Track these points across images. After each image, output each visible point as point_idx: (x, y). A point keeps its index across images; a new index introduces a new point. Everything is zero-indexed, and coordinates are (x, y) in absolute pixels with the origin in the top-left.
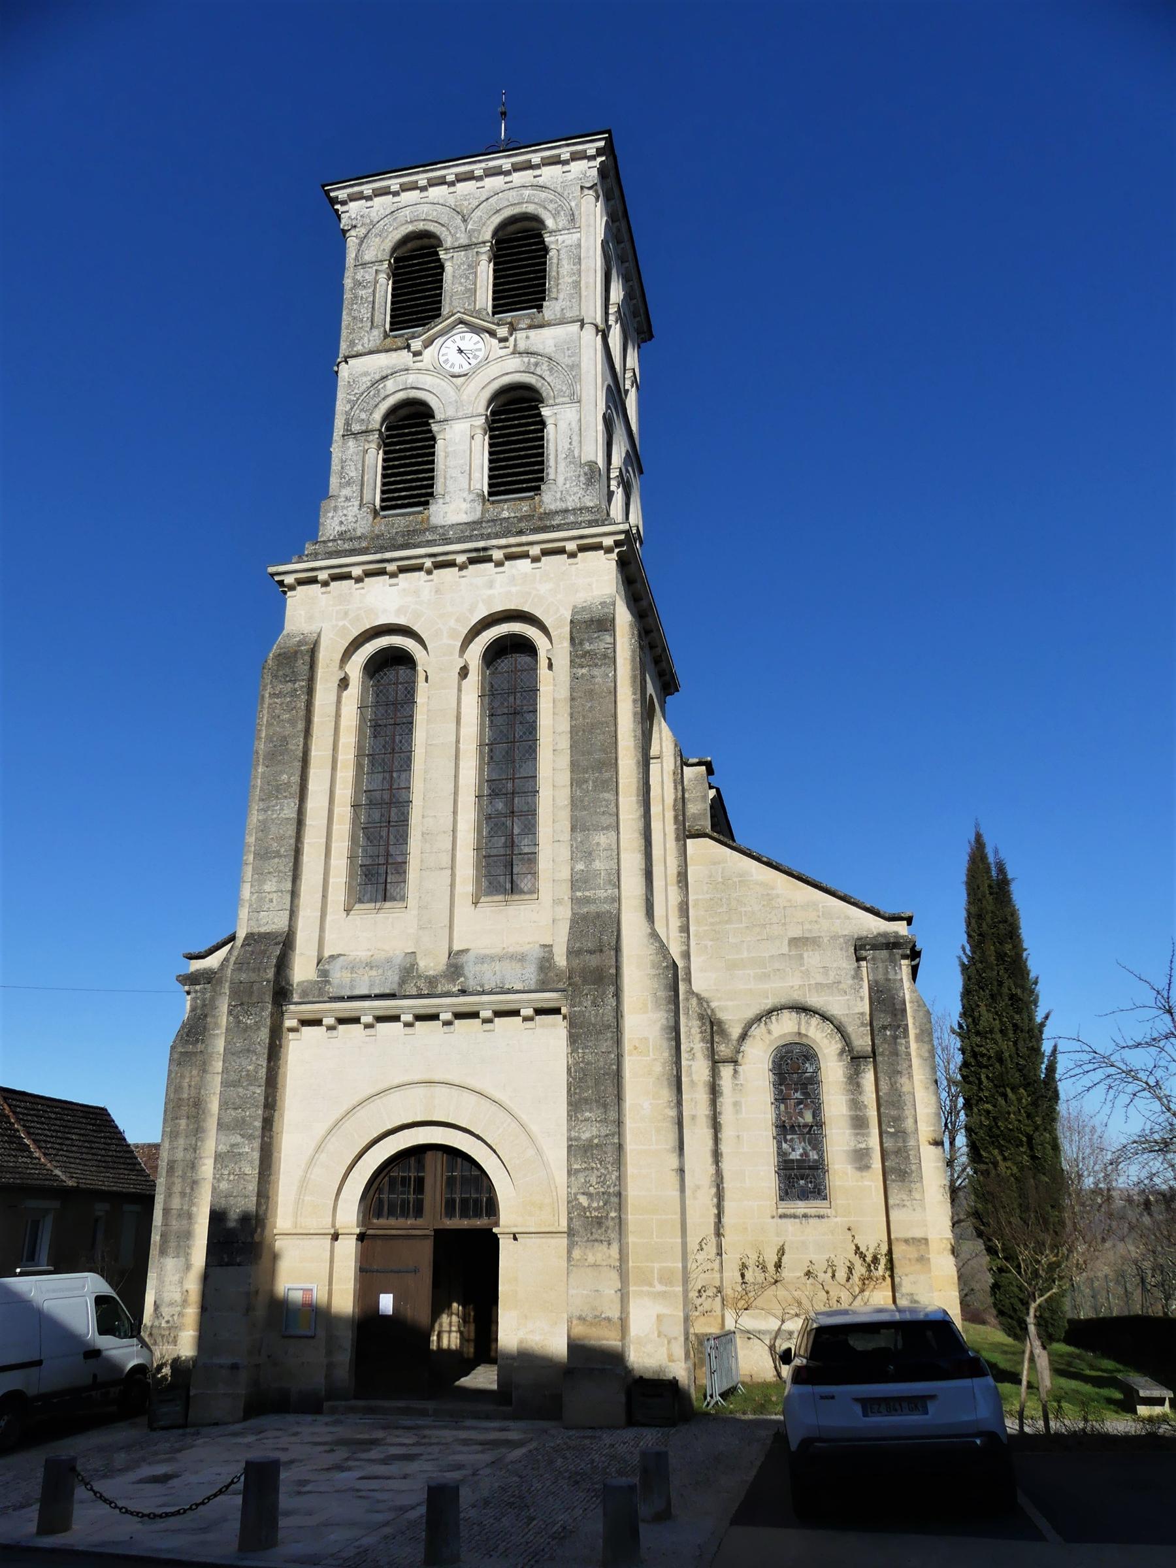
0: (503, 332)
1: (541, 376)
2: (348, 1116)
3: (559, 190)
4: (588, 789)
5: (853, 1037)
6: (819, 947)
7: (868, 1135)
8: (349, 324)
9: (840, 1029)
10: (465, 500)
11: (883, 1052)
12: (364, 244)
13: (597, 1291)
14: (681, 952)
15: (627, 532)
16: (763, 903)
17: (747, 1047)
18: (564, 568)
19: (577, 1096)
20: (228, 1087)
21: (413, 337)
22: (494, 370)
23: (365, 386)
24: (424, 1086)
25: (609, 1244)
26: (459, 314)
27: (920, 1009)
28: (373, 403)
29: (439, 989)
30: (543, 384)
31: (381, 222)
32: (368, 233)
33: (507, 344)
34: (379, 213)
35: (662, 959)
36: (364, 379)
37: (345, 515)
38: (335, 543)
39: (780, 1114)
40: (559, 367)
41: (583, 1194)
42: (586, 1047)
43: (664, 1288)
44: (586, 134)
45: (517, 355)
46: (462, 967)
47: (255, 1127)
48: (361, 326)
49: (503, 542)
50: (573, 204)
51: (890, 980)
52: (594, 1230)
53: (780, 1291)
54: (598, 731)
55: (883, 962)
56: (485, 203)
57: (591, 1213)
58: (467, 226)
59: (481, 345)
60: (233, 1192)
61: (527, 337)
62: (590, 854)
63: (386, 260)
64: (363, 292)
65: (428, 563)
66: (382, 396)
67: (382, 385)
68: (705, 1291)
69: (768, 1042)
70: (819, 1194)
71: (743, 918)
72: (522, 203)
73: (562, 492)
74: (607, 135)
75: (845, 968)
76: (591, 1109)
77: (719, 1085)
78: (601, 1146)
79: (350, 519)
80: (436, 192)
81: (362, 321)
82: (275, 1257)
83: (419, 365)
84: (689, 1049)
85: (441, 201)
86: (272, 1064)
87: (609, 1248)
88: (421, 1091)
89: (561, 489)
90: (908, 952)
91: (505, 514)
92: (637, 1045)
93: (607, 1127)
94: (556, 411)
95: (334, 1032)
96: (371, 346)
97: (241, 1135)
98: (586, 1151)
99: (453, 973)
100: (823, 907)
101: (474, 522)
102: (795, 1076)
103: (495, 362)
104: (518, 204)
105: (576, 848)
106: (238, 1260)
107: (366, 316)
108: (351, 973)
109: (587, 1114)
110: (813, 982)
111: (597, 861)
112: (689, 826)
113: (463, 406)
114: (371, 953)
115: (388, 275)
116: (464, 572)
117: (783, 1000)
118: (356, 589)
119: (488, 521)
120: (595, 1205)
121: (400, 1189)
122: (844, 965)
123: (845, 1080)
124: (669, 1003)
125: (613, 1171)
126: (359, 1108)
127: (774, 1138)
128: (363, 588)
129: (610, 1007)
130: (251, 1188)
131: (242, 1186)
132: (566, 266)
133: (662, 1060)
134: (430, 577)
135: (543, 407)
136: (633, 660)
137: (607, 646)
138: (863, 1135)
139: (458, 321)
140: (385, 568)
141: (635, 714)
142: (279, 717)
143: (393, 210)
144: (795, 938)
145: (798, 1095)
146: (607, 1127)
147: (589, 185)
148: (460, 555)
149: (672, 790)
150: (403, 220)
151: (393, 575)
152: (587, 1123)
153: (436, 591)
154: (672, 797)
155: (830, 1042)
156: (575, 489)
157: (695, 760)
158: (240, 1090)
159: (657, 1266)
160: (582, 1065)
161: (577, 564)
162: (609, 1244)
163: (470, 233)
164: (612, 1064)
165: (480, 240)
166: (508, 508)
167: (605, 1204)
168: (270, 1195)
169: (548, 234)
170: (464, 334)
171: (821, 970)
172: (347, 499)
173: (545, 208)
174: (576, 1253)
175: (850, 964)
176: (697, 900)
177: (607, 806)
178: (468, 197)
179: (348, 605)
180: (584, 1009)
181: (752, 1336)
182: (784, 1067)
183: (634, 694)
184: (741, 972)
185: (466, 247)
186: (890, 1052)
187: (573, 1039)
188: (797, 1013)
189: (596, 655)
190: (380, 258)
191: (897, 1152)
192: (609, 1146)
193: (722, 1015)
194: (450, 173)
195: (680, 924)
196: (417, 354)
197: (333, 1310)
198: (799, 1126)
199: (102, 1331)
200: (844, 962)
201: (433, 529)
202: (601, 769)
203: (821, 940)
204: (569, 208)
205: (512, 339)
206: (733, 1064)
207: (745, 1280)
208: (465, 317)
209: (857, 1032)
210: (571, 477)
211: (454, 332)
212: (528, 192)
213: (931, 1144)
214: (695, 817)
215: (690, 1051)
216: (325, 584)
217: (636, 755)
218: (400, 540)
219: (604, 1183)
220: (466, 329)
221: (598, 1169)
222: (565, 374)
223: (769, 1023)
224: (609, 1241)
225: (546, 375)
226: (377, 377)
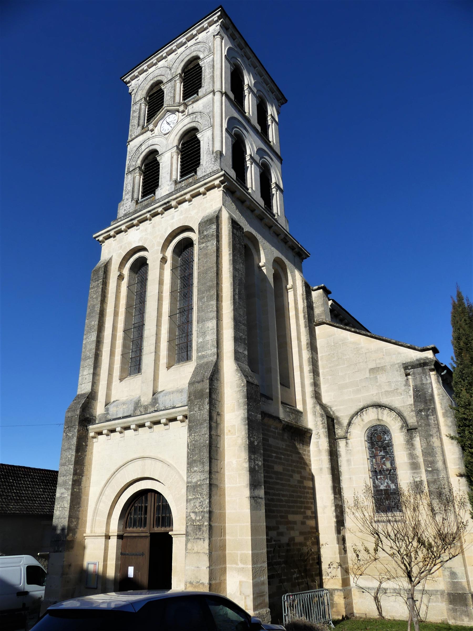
1: (197, 122)
2: (113, 477)
3: (205, 41)
5: (408, 418)
6: (385, 371)
7: (420, 473)
9: (400, 414)
10: (168, 185)
11: (421, 424)
13: (198, 567)
14: (311, 383)
15: (223, 175)
16: (354, 352)
17: (352, 429)
18: (201, 201)
19: (191, 459)
20: (61, 466)
24: (141, 460)
25: (204, 540)
27: (444, 398)
29: (149, 411)
30: (198, 125)
33: (184, 113)
35: (241, 382)
39: (373, 465)
40: (204, 115)
41: (193, 512)
42: (196, 433)
43: (243, 566)
44: (211, 13)
46: (158, 399)
47: (69, 484)
49: (174, 196)
51: (424, 384)
52: (197, 533)
53: (378, 564)
54: (209, 272)
55: (419, 375)
57: (196, 523)
60: (60, 516)
62: (205, 333)
66: (140, 153)
68: (332, 565)
69: (362, 426)
70: (398, 508)
71: (345, 362)
75: (400, 381)
76: (197, 465)
77: (339, 451)
78: (201, 485)
79: (128, 207)
80: (161, 64)
82: (84, 548)
83: (153, 135)
84: (317, 433)
85: (163, 66)
86: (80, 454)
87: (204, 543)
88: (140, 462)
90: (433, 367)
92: (230, 430)
93: (204, 475)
95: (109, 437)
97: (65, 488)
98: (194, 489)
99: (154, 402)
100: (386, 350)
102: (380, 443)
105: (199, 331)
106: (60, 549)
109: (195, 469)
110: (383, 391)
111: (208, 336)
112: (316, 320)
115: (145, 104)
116: (163, 215)
117: (369, 402)
120: (198, 518)
121: (139, 513)
122: (399, 379)
123: (405, 443)
124: (245, 405)
125: (206, 499)
126: (117, 473)
127: (370, 478)
129: (206, 410)
130: (66, 514)
131: (63, 513)
133: (242, 437)
137: (213, 230)
138: (418, 473)
139: (166, 111)
141: (230, 260)
144: (372, 369)
145: (382, 453)
146: (204, 475)
147: (216, 34)
149: (302, 303)
151: (137, 225)
152: (195, 473)
154: (302, 306)
155: (395, 422)
156: (210, 165)
157: (316, 287)
158: (66, 467)
159: (239, 552)
160: (193, 442)
162: (204, 540)
164: (206, 441)
167: (202, 518)
168: (80, 517)
171: (387, 384)
172: (127, 199)
174: (189, 545)
175: (403, 378)
176: (322, 356)
177: (212, 308)
180: (195, 412)
181: (364, 591)
182: (373, 439)
183: (230, 251)
184: (346, 390)
185: (170, 80)
186: (425, 424)
187: (190, 429)
188: (376, 408)
189: (208, 236)
191: (434, 482)
192: (205, 486)
193: (338, 414)
194: (164, 53)
195: (309, 369)
196: (152, 130)
197: (107, 575)
198: (384, 470)
199: (29, 582)
200: (399, 377)
202: (210, 290)
203: (386, 367)
206: (345, 439)
207: (359, 559)
208: (168, 108)
209: (409, 415)
210: (209, 160)
211: (166, 116)
213: (458, 476)
214: (319, 315)
215: (318, 434)
217: (230, 281)
219: (202, 506)
220: (170, 114)
221: (199, 499)
223: (362, 415)
224: (204, 538)
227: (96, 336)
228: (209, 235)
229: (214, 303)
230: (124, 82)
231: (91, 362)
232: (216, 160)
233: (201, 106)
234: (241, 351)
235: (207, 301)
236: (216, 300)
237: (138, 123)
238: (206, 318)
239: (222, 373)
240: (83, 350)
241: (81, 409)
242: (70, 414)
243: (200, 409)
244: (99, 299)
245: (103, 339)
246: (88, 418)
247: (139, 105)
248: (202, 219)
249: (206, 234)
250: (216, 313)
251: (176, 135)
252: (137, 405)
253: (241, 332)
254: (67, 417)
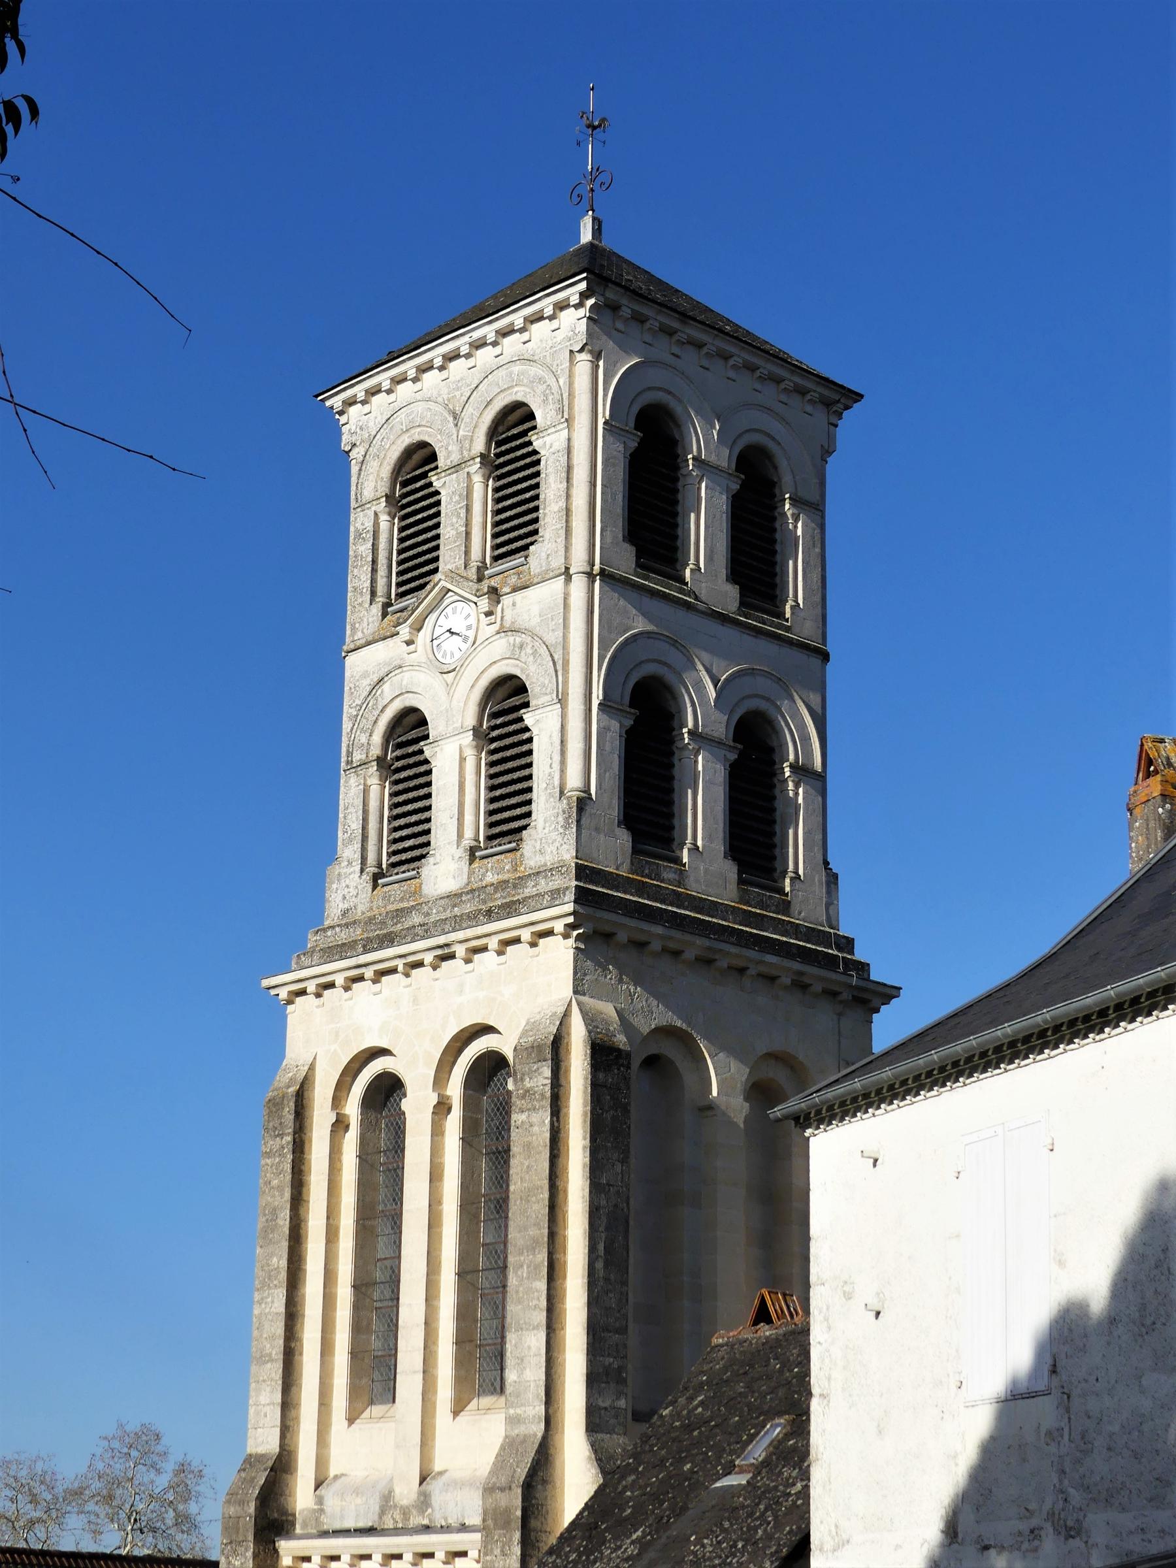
4: (523, 1277)
22: (481, 660)
46: (430, 1495)
54: (534, 1199)
58: (458, 431)
62: (522, 1360)
63: (382, 497)
65: (400, 964)
66: (380, 708)
67: (379, 691)
94: (537, 717)
103: (483, 646)
104: (508, 388)
108: (341, 1500)
111: (528, 1370)
114: (367, 1474)
115: (389, 514)
132: (553, 486)
136: (585, 1092)
142: (270, 1182)
147: (578, 348)
148: (427, 952)
178: (460, 384)
180: (494, 1558)
202: (534, 1249)
211: (446, 602)
227: (284, 1301)
228: (535, 1092)
229: (542, 1285)
231: (275, 1370)
232: (566, 827)
233: (535, 610)
234: (607, 1404)
235: (528, 1278)
236: (546, 1280)
237: (372, 586)
238: (525, 1323)
239: (558, 1463)
240: (255, 1333)
241: (258, 1502)
242: (232, 1511)
243: (504, 1554)
244: (287, 1195)
245: (303, 1305)
246: (276, 1520)
247: (371, 514)
248: (524, 1033)
249: (528, 1085)
250: (545, 1313)
251: (472, 686)
252: (387, 1502)
253: (609, 1355)
254: (227, 1516)
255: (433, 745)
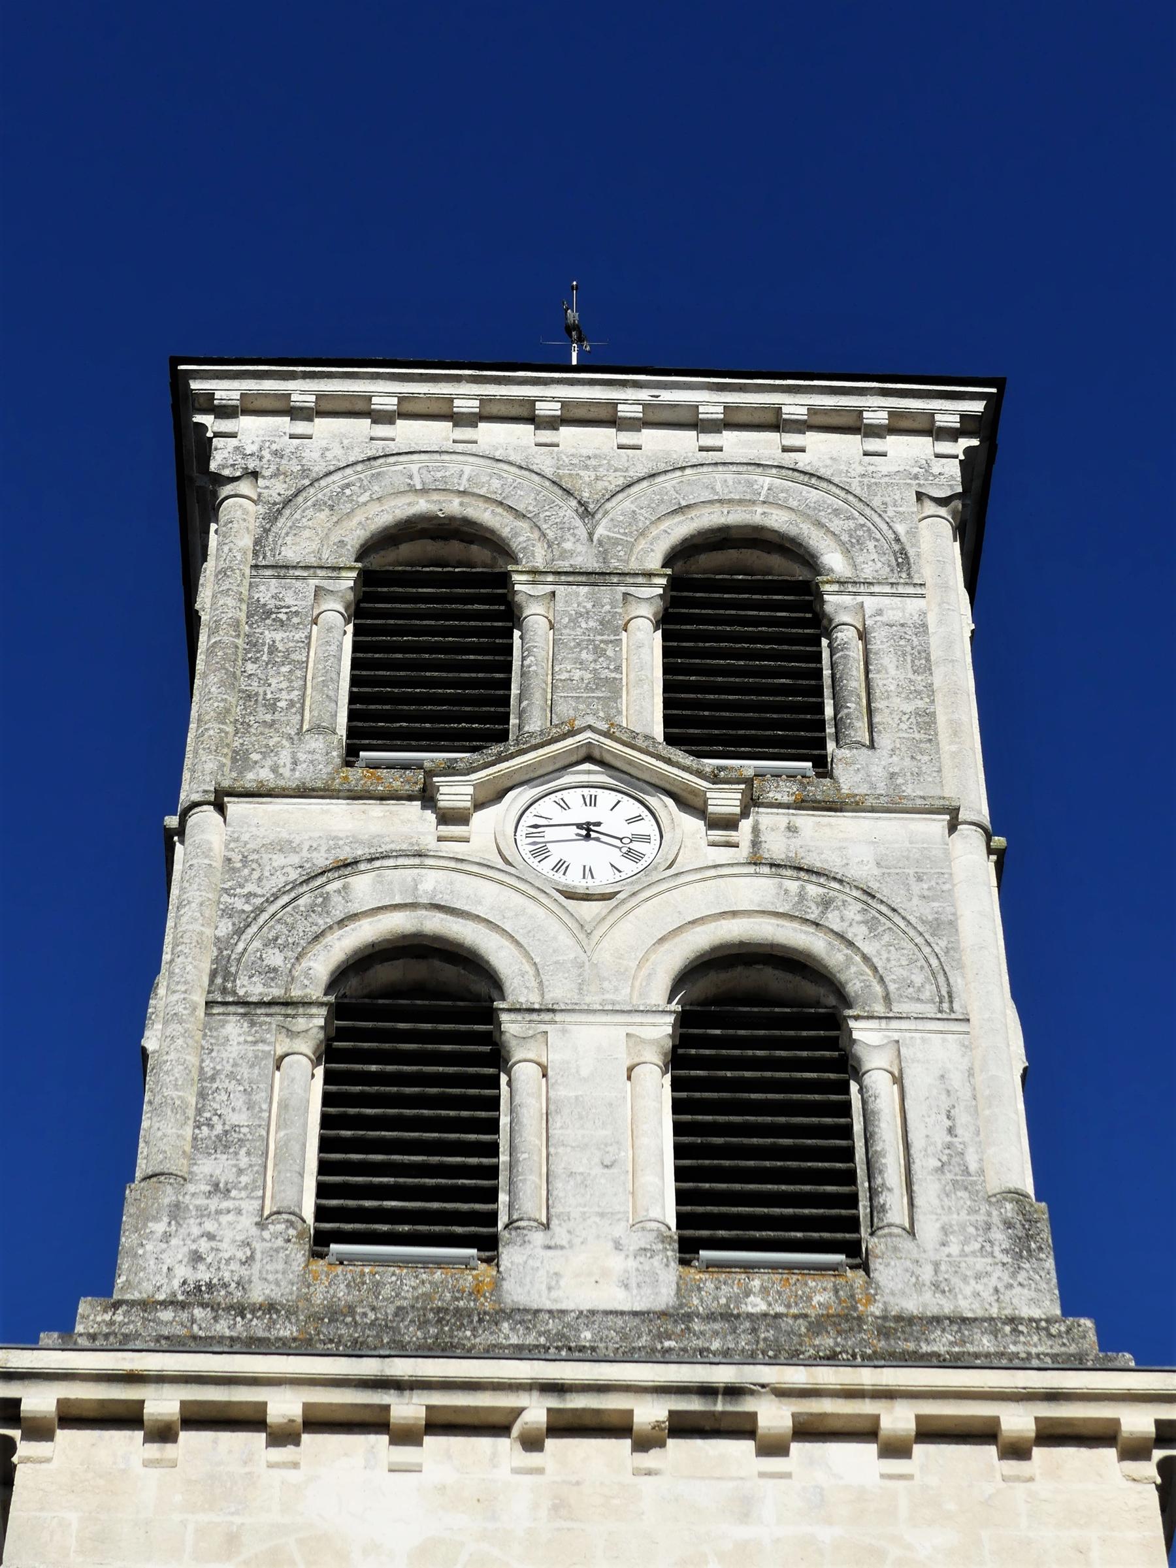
0: (725, 801)
1: (841, 936)
8: (228, 711)
12: (282, 520)
21: (450, 770)
23: (281, 881)
26: (589, 734)
28: (305, 928)
31: (336, 477)
32: (296, 495)
33: (733, 836)
34: (329, 455)
36: (279, 860)
37: (211, 1237)
38: (184, 1316)
40: (897, 919)
45: (766, 870)
48: (268, 718)
49: (796, 1376)
50: (901, 529)
56: (645, 484)
58: (594, 527)
59: (647, 826)
61: (791, 829)
64: (278, 636)
66: (339, 914)
67: (337, 885)
72: (754, 502)
73: (936, 1265)
74: (994, 390)
79: (228, 1249)
81: (272, 706)
89: (933, 1256)
91: (756, 1305)
96: (303, 774)
101: (663, 1314)
103: (699, 876)
104: (740, 502)
107: (284, 695)
113: (602, 979)
118: (270, 1466)
119: (711, 1317)
128: (295, 1465)
132: (892, 671)
134: (534, 1459)
135: (857, 1018)
139: (582, 753)
140: (387, 1408)
143: (370, 454)
148: (648, 1398)
150: (400, 482)
151: (406, 1436)
153: (555, 1508)
161: (1031, 1479)
163: (604, 548)
165: (633, 566)
166: (764, 1291)
169: (835, 587)
170: (593, 791)
173: (819, 524)
178: (593, 462)
179: (236, 1513)
185: (595, 578)
190: (328, 557)
196: (458, 817)
201: (526, 1316)
204: (891, 536)
205: (745, 825)
210: (963, 1227)
211: (567, 779)
212: (768, 480)
216: (163, 1434)
218: (412, 1334)
222: (919, 940)
225: (858, 933)
226: (322, 860)
230: (179, 382)
255: (535, 1017)
